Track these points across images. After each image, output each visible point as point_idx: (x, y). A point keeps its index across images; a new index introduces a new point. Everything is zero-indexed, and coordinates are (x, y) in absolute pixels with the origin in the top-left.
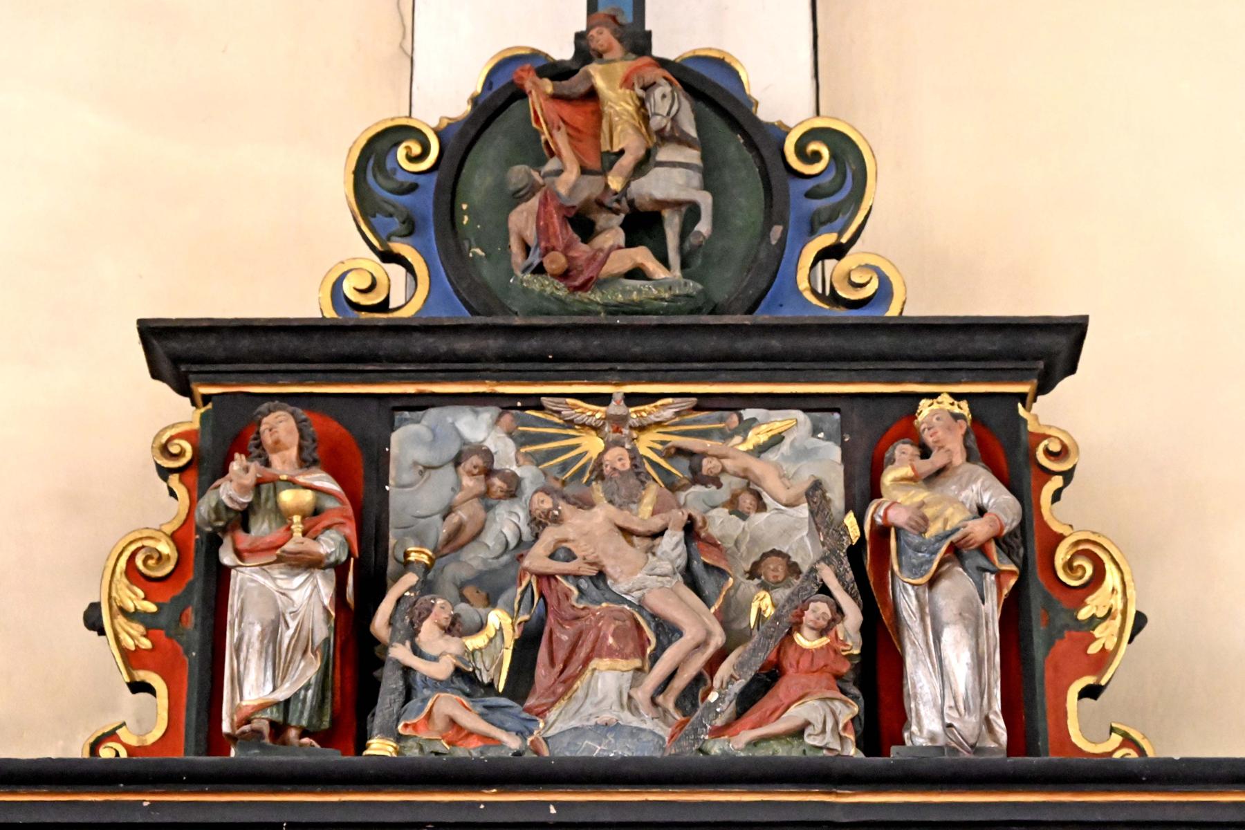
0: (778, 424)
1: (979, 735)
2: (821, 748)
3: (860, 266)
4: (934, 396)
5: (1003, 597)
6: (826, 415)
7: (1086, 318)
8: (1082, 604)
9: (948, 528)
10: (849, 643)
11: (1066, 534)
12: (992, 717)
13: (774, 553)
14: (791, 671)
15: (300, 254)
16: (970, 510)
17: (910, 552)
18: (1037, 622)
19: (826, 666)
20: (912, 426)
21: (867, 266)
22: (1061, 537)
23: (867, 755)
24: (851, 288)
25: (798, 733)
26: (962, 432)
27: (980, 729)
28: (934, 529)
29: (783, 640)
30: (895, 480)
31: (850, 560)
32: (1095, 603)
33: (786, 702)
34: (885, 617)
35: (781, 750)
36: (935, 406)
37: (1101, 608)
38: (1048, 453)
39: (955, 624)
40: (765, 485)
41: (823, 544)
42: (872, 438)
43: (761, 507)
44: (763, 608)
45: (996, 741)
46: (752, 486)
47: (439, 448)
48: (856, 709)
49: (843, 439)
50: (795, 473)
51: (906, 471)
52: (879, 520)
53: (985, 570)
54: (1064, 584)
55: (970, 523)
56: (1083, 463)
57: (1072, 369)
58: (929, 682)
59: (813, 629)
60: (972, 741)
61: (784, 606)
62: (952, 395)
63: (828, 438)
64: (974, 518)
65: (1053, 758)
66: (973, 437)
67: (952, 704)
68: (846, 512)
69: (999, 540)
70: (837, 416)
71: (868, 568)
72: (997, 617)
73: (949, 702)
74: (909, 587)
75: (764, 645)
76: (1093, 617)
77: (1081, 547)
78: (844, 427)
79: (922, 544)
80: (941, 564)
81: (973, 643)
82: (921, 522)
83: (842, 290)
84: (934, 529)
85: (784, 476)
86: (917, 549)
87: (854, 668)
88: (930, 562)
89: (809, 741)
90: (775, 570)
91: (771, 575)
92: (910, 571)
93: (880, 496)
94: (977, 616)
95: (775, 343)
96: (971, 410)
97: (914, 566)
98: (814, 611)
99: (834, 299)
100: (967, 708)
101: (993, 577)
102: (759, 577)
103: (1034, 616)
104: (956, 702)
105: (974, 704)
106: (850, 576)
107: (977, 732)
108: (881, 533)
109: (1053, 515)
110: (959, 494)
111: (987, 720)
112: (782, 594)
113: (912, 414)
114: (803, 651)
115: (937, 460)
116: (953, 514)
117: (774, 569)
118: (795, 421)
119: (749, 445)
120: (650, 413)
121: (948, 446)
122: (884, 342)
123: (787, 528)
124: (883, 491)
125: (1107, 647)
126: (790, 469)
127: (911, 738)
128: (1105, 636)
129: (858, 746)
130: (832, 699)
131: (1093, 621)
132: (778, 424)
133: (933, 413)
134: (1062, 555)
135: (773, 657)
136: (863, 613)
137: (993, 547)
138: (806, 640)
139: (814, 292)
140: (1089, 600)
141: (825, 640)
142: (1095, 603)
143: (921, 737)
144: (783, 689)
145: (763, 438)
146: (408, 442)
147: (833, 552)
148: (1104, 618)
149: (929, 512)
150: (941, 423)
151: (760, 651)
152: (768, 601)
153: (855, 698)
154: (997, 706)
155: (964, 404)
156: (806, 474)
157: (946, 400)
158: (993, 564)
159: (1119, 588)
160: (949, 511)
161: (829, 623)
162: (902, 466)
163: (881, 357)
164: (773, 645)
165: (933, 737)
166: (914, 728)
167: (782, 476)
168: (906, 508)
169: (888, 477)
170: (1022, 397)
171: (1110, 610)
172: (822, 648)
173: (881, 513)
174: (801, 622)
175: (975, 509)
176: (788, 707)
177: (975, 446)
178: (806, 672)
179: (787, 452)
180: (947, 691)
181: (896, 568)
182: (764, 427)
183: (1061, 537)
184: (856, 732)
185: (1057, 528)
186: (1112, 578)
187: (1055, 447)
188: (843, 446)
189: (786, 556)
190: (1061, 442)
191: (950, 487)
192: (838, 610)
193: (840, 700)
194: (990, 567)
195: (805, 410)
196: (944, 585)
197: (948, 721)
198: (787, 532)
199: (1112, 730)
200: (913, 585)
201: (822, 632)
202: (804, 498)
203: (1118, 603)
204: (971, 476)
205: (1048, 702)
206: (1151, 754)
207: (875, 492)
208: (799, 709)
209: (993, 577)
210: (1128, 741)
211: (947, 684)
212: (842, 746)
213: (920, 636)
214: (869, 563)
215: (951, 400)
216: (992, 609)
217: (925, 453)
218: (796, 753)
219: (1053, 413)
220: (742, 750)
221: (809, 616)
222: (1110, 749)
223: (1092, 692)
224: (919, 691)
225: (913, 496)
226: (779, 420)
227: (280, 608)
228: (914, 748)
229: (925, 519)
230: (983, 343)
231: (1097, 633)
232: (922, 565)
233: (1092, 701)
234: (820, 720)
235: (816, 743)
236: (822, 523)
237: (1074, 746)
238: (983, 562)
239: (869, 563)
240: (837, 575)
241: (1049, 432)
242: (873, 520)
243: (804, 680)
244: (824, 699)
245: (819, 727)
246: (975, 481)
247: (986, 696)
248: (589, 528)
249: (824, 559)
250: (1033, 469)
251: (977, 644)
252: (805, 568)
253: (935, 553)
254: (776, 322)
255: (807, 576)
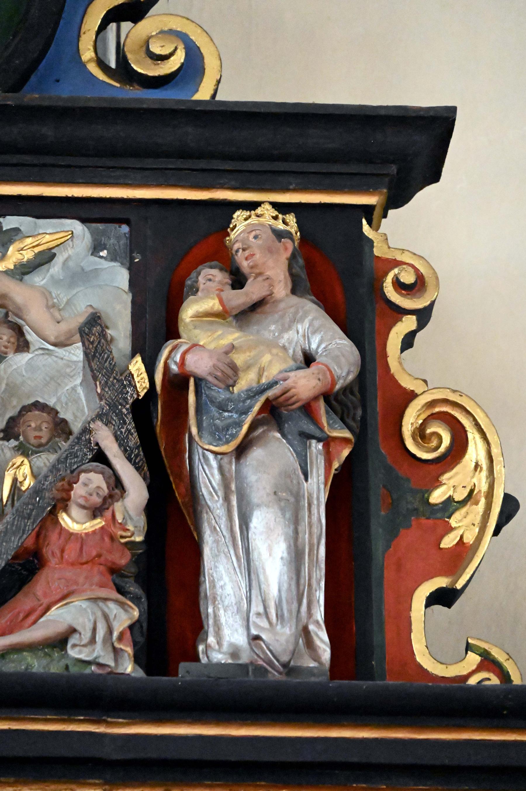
0: (48, 238)
1: (293, 653)
2: (88, 663)
3: (162, 32)
4: (252, 206)
5: (333, 471)
6: (112, 227)
7: (453, 110)
8: (436, 483)
9: (264, 381)
10: (131, 527)
11: (418, 391)
12: (311, 627)
13: (37, 406)
14: (53, 562)
16: (294, 359)
17: (214, 411)
18: (375, 504)
19: (99, 556)
20: (223, 243)
21: (171, 32)
22: (412, 396)
23: (149, 672)
24: (149, 61)
25: (60, 642)
26: (288, 254)
27: (297, 643)
28: (246, 381)
29: (44, 520)
30: (198, 316)
31: (135, 419)
32: (452, 482)
33: (45, 602)
34: (179, 493)
35: (36, 664)
36: (253, 220)
37: (460, 489)
38: (398, 285)
39: (268, 506)
40: (27, 318)
41: (101, 397)
42: (169, 257)
43: (23, 346)
44: (20, 479)
45: (316, 658)
46: (12, 318)
48: (136, 613)
49: (132, 259)
50: (68, 303)
51: (212, 304)
52: (174, 368)
53: (311, 437)
54: (414, 456)
55: (292, 374)
56: (445, 298)
57: (434, 176)
58: (231, 580)
59: (83, 507)
60: (285, 658)
61: (46, 477)
62: (275, 205)
63: (113, 257)
64: (299, 368)
65: (390, 682)
66: (301, 261)
67: (261, 610)
68: (133, 356)
69: (328, 397)
70: (125, 229)
71: (158, 430)
72: (323, 498)
73: (257, 607)
74: (211, 456)
75: (18, 528)
76: (450, 499)
77: (437, 410)
78: (135, 243)
79: (229, 400)
80: (253, 427)
81: (290, 531)
82: (230, 372)
83: (138, 62)
84: (246, 381)
85: (54, 306)
86: (222, 407)
87: (136, 560)
88: (239, 425)
89: (73, 653)
90: (39, 428)
91: (32, 434)
92: (212, 434)
93: (177, 336)
94: (298, 496)
95: (48, 131)
96: (300, 227)
97: (217, 429)
98: (85, 485)
99: (124, 72)
100: (280, 616)
101: (320, 446)
102: (17, 438)
103: (373, 500)
104: (265, 608)
105: (290, 611)
106: (134, 439)
107: (291, 647)
108: (178, 384)
109: (403, 367)
110: (280, 336)
111: (306, 632)
112: (45, 460)
113: (224, 228)
114: (70, 535)
115: (253, 291)
116: (270, 362)
117: (36, 427)
118: (71, 235)
119: (9, 264)
121: (268, 273)
122: (191, 134)
124: (181, 330)
125: (465, 540)
126: (61, 296)
127: (206, 653)
128: (463, 525)
129: (137, 660)
130: (105, 600)
131: (450, 506)
132: (48, 238)
133: (250, 229)
134: (411, 419)
135: (30, 543)
136: (150, 488)
137: (321, 407)
138: (74, 522)
139: (102, 64)
140: (444, 478)
141: (99, 523)
142: (452, 482)
143: (219, 651)
144: (43, 584)
145: (28, 255)
147: (113, 406)
148: (463, 503)
149: (239, 359)
150: (259, 242)
151: (14, 533)
152: (26, 469)
153: (136, 600)
154: (319, 613)
155: (291, 218)
156: (82, 303)
157: (267, 211)
158: (322, 430)
159: (484, 463)
160: (266, 358)
161: (105, 499)
162: (207, 296)
163: (184, 154)
164: (31, 526)
165: (235, 653)
166: (211, 640)
167: (51, 307)
168: (211, 352)
169: (189, 311)
170: (367, 211)
171: (472, 491)
172: (94, 532)
173: (178, 358)
174: (69, 499)
175: (300, 356)
176: (48, 609)
177: (304, 275)
178: (73, 564)
180: (254, 592)
181: (194, 430)
182: (29, 241)
183: (412, 396)
184: (135, 644)
185: (407, 383)
186: (475, 451)
187: (408, 278)
188: (132, 269)
189: (52, 411)
190: (416, 270)
191: (269, 328)
192: (117, 485)
193: (116, 601)
194: (318, 433)
195: (84, 221)
196: (256, 454)
197: (254, 632)
198: (56, 379)
199: (469, 647)
200: (215, 453)
201: (95, 512)
202: (78, 336)
203: (481, 482)
204: (296, 313)
205: (389, 597)
206: (516, 680)
207: (172, 332)
208: (61, 611)
209: (320, 446)
210: (488, 662)
211: (254, 583)
212: (116, 660)
213: (223, 522)
214: (158, 427)
215: (275, 213)
216: (317, 488)
217: (238, 280)
218: (55, 668)
219: (409, 232)
220: (132, 558)
221: (78, 491)
222: (465, 673)
223: (444, 598)
224: (219, 591)
225: (220, 337)
226: (41, 234)
228: (210, 665)
229: (234, 368)
230: (317, 138)
231: (453, 522)
232: (227, 428)
233: (446, 608)
234: (89, 626)
235: (82, 656)
236: (100, 370)
237: (420, 666)
238: (311, 428)
239: (158, 427)
240: (117, 438)
241: (399, 257)
242: (166, 367)
243: (69, 573)
244: (95, 600)
245: (86, 636)
246: (301, 320)
247: (305, 601)
249: (100, 416)
250: (380, 306)
251: (296, 532)
252: (76, 427)
253: (245, 412)
254: (46, 103)
255: (79, 438)
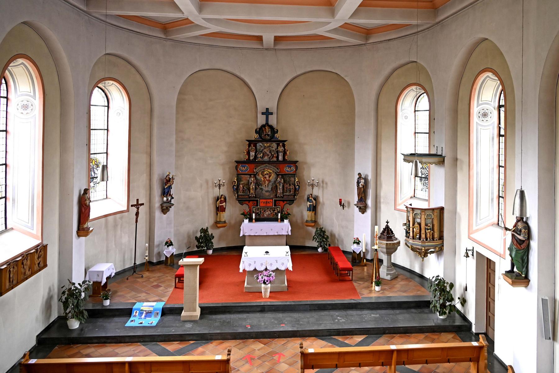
15: (255, 136)
18: (285, 153)
42: (278, 145)
47: (259, 145)
120: (308, 322)
123: (274, 149)
146: (258, 145)
179: (274, 145)
227: (252, 154)
248: (265, 150)
